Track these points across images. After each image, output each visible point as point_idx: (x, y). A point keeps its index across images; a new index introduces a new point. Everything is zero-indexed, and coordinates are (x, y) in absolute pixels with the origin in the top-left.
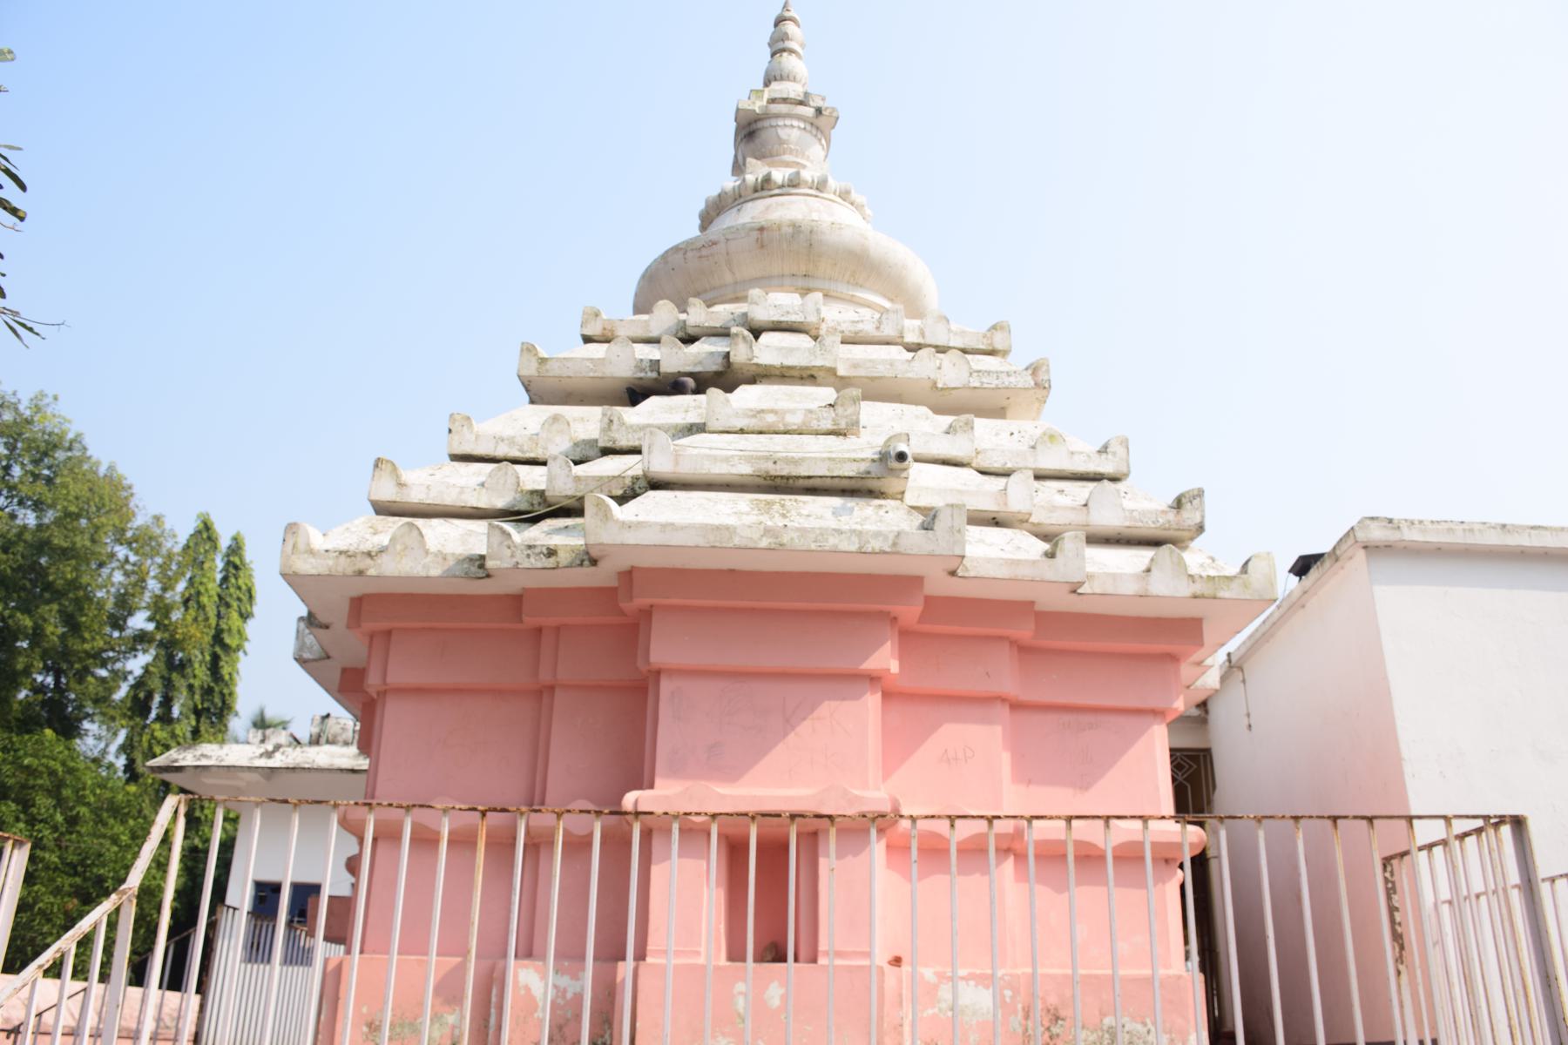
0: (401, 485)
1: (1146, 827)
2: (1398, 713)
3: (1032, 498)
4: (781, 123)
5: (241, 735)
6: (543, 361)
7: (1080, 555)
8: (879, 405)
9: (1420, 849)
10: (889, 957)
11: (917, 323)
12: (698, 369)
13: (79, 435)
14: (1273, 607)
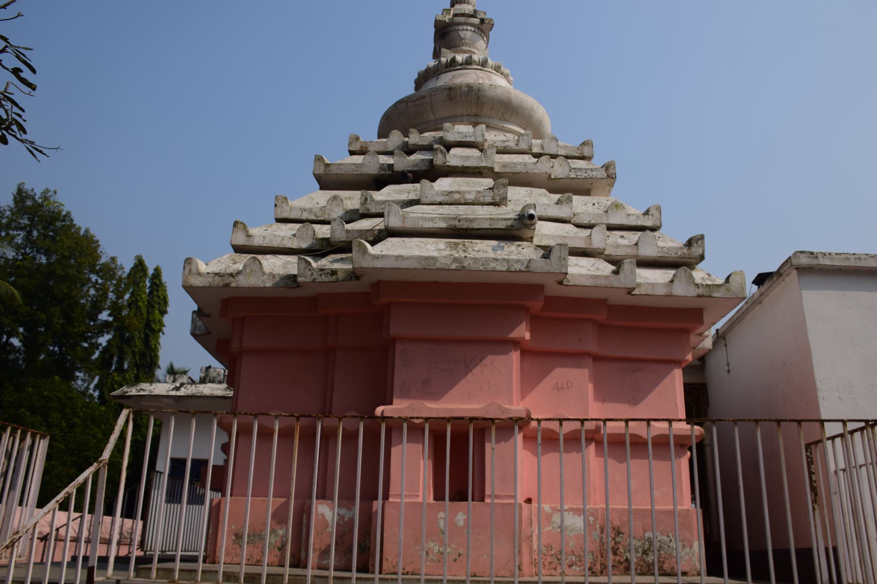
0: (249, 236)
1: (670, 425)
2: (814, 363)
4: (460, 28)
5: (161, 378)
6: (327, 165)
8: (518, 188)
9: (828, 439)
10: (525, 499)
11: (539, 141)
12: (416, 169)
13: (68, 213)
14: (743, 303)
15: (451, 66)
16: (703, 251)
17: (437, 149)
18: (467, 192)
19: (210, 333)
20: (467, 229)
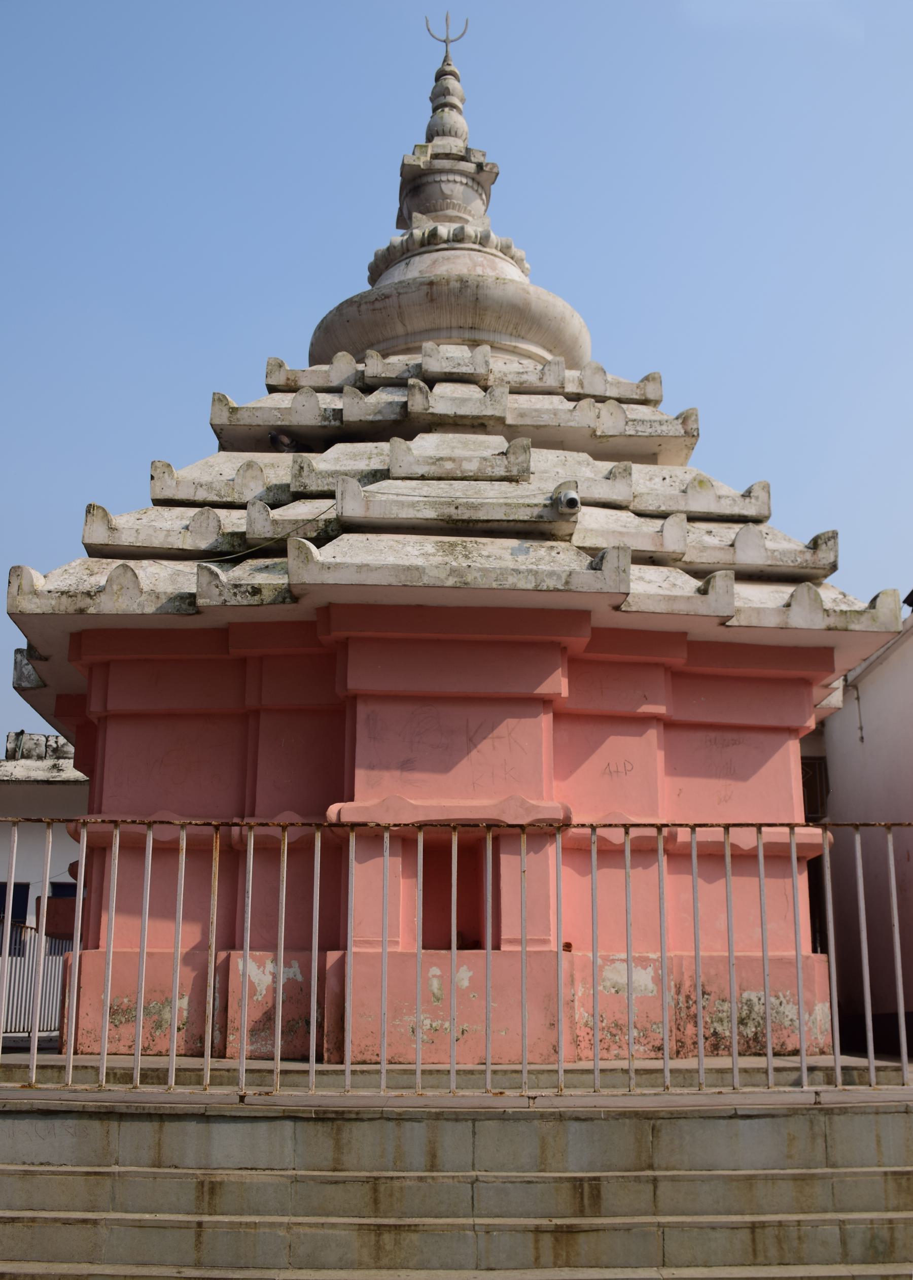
0: (112, 529)
3: (685, 540)
4: (444, 178)
6: (234, 410)
7: (730, 593)
15: (429, 244)
16: (836, 557)
17: (413, 386)
18: (466, 459)
19: (45, 686)
20: (468, 521)
